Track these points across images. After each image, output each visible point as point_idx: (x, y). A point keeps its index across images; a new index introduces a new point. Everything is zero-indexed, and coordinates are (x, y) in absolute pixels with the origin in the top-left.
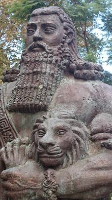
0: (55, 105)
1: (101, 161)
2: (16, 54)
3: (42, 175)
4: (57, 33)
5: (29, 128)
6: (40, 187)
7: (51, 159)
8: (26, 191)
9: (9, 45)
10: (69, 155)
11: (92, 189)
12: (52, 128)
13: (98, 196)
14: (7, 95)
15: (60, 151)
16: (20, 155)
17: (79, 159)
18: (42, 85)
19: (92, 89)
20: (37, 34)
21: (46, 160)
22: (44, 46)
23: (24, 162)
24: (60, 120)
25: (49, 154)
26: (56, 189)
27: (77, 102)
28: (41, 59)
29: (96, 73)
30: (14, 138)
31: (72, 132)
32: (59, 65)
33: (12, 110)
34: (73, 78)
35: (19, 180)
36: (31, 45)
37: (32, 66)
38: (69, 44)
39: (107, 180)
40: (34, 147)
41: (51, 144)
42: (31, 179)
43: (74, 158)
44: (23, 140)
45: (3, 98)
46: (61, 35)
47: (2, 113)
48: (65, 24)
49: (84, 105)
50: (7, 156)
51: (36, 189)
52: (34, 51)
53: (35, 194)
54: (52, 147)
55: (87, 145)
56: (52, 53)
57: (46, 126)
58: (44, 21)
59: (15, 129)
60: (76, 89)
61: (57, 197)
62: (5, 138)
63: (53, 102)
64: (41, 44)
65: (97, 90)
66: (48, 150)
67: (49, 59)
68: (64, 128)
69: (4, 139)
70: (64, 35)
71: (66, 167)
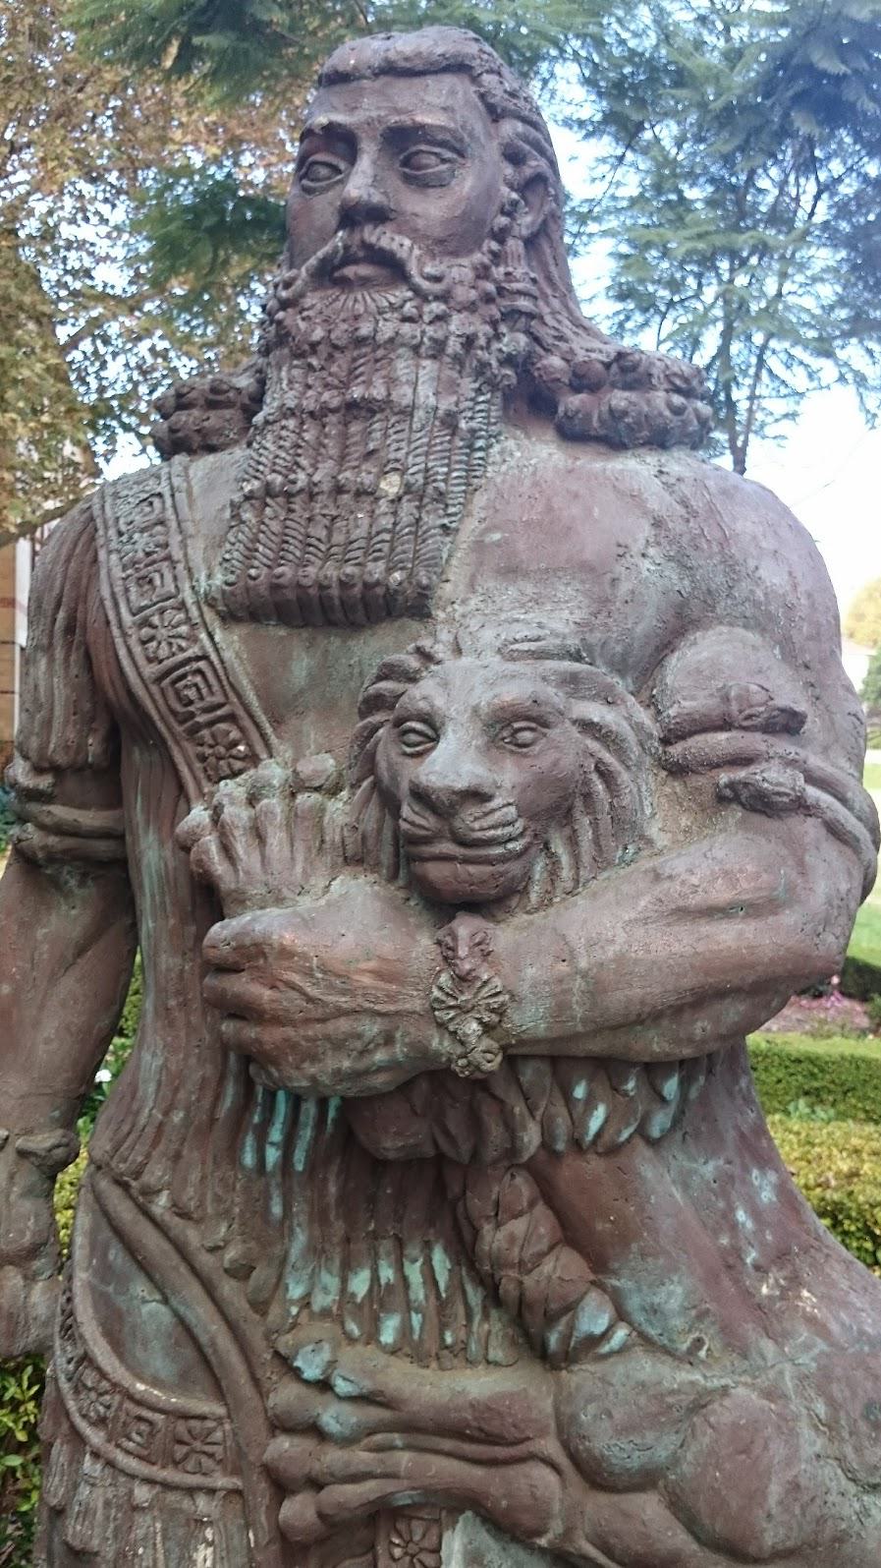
0: (472, 586)
1: (726, 873)
2: (88, 262)
3: (424, 945)
4: (466, 183)
5: (328, 708)
6: (417, 1005)
7: (472, 869)
8: (343, 1025)
9: (50, 213)
10: (559, 847)
11: (677, 1011)
12: (476, 710)
13: (704, 1041)
15: (520, 825)
16: (299, 846)
17: (609, 864)
18: (395, 478)
19: (658, 499)
20: (360, 183)
21: (438, 868)
22: (402, 254)
23: (322, 883)
24: (511, 666)
25: (463, 843)
26: (500, 1011)
27: (588, 570)
28: (387, 330)
29: (678, 411)
30: (253, 759)
31: (574, 731)
32: (484, 365)
33: (244, 608)
34: (550, 434)
35: (308, 973)
36: (327, 249)
38: (531, 242)
39: (752, 966)
40: (373, 811)
41: (476, 796)
42: (372, 965)
43: (586, 859)
44: (306, 768)
45: (184, 545)
46: (489, 192)
47: (184, 629)
49: (624, 587)
50: (227, 850)
51: (397, 1013)
52: (345, 284)
53: (389, 1040)
54: (476, 810)
55: (649, 796)
56: (444, 297)
58: (398, 111)
59: (263, 719)
60: (576, 496)
61: (504, 1048)
62: (203, 758)
64: (384, 243)
65: (684, 503)
66: (457, 823)
67: (430, 330)
69: (198, 765)
70: (505, 190)
71: (546, 903)
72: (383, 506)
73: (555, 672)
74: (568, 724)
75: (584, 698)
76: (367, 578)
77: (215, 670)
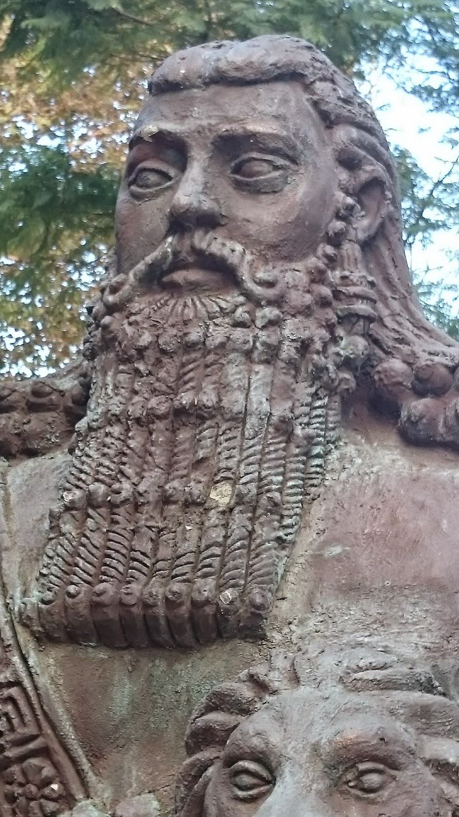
0: (310, 605)
4: (300, 190)
14: (20, 543)
18: (226, 488)
20: (190, 189)
22: (234, 259)
28: (218, 335)
31: (428, 774)
33: (59, 629)
34: (393, 439)
36: (155, 254)
37: (168, 371)
38: (368, 245)
46: (324, 197)
48: (343, 134)
52: (174, 289)
56: (278, 302)
57: (275, 738)
60: (422, 507)
63: (294, 591)
64: (215, 248)
67: (263, 336)
68: (382, 752)
70: (340, 195)
72: (214, 518)
73: (404, 705)
74: (420, 765)
75: (436, 734)
76: (196, 596)
77: (31, 705)
